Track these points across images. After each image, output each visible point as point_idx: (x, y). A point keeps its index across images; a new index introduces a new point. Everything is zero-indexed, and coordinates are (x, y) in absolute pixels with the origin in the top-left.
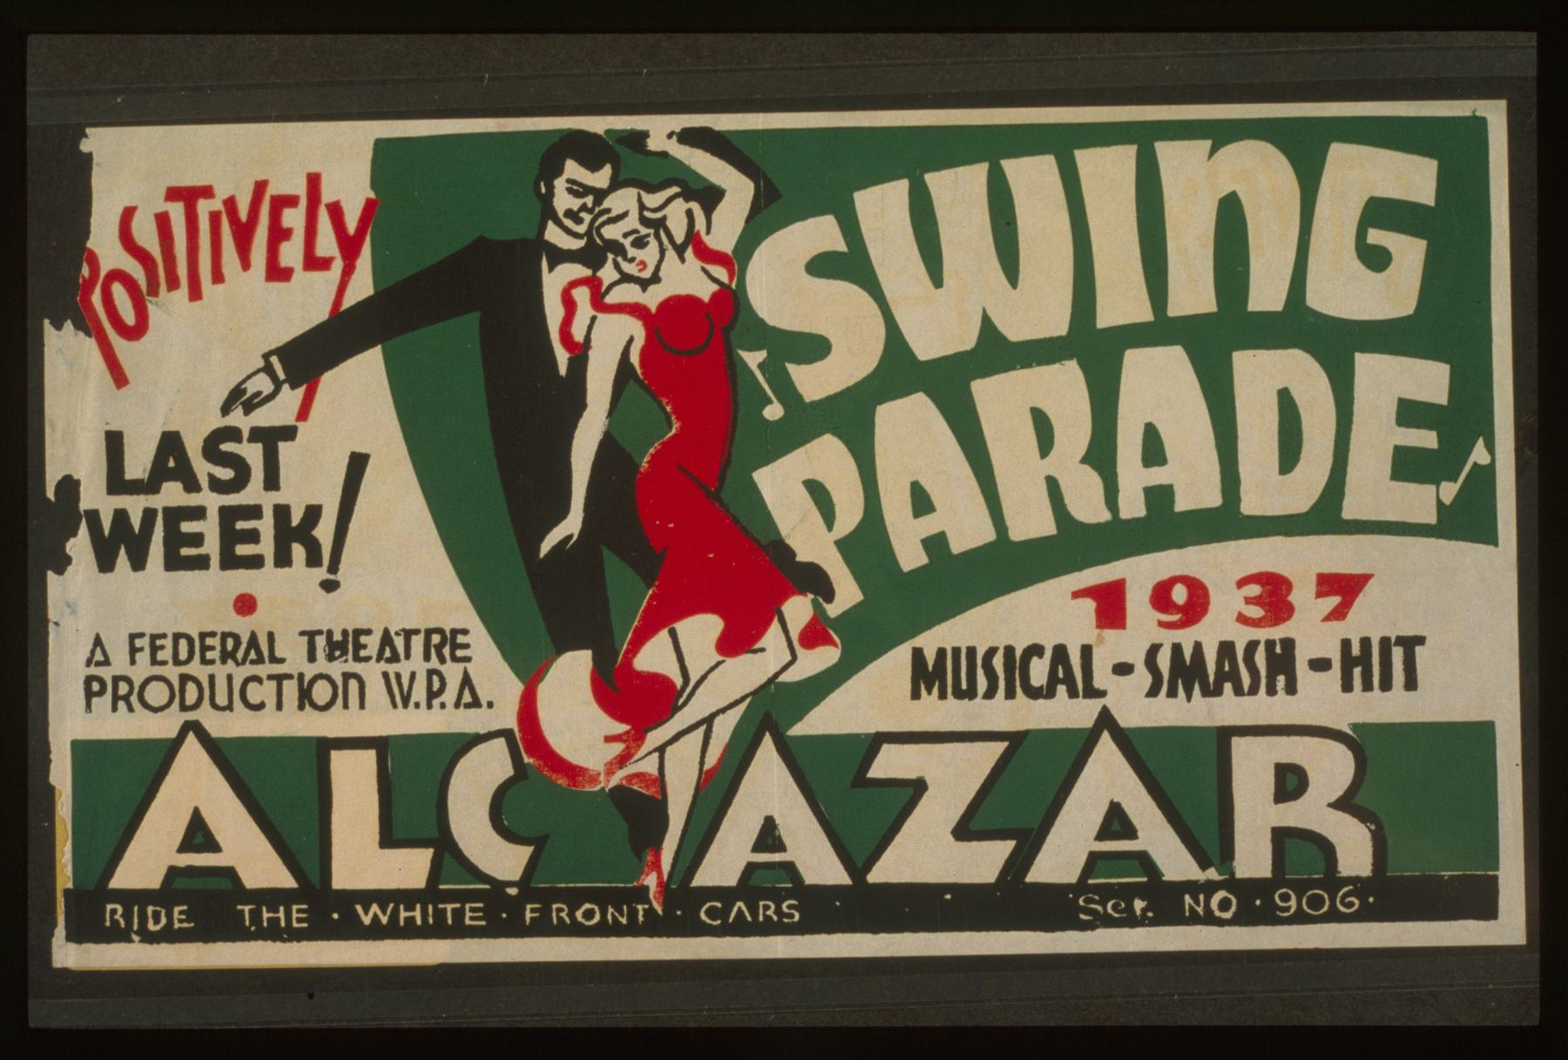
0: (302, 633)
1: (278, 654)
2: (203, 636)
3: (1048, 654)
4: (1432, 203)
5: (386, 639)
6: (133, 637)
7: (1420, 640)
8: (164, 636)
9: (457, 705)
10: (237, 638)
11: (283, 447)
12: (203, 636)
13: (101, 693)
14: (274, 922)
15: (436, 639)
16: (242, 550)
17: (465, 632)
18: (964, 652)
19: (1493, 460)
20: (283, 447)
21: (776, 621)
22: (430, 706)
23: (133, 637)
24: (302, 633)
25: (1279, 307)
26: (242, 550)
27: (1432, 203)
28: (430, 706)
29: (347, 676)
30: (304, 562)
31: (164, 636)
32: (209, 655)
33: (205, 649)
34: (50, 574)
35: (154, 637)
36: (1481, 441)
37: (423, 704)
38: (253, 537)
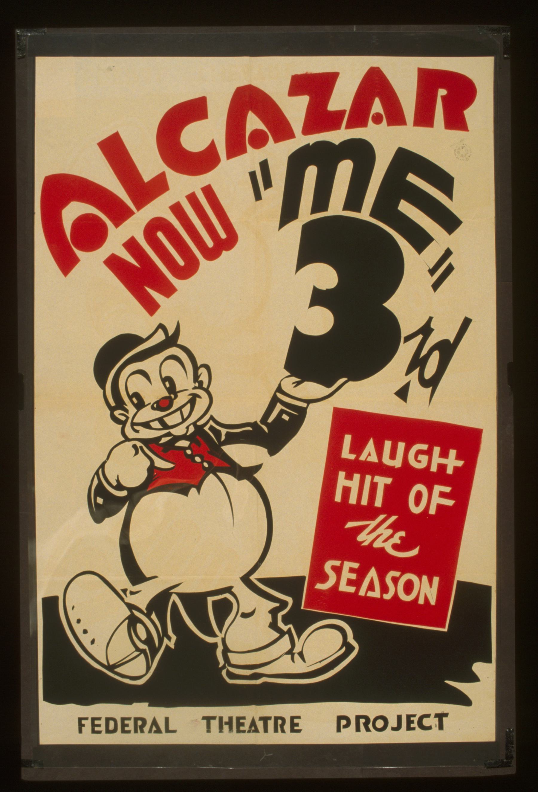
0: (204, 718)
2: (123, 719)
3: (153, 731)
5: (253, 723)
6: (80, 720)
7: (446, 715)
8: (129, 719)
10: (144, 721)
11: (444, 719)
12: (123, 719)
13: (347, 725)
14: (413, 722)
16: (97, 729)
17: (299, 717)
18: (139, 731)
19: (190, 425)
20: (444, 719)
23: (80, 720)
26: (97, 729)
30: (349, 578)
31: (129, 719)
33: (124, 725)
35: (93, 719)
36: (418, 369)
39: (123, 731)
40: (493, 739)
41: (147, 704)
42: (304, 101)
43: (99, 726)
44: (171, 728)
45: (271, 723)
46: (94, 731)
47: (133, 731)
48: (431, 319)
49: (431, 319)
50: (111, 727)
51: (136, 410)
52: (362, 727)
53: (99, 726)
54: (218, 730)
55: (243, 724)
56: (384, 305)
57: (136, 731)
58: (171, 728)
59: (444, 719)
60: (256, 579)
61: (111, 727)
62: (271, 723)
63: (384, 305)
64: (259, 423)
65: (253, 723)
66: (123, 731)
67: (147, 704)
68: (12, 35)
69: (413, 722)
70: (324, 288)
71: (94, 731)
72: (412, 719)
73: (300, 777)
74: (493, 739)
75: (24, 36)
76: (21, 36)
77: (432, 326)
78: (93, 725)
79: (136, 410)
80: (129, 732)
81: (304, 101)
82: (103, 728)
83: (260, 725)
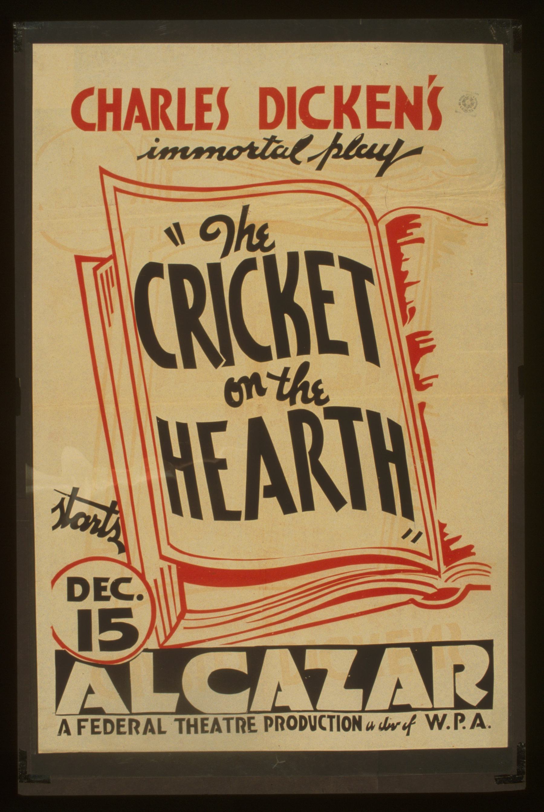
0: (164, 732)
1: (177, 723)
4: (325, 304)
5: (216, 722)
9: (472, 727)
11: (215, 436)
13: (271, 725)
15: (241, 723)
16: (96, 730)
20: (215, 436)
21: (248, 691)
22: (456, 728)
24: (164, 732)
25: (275, 498)
26: (96, 730)
27: (325, 304)
28: (456, 728)
29: (277, 718)
32: (122, 729)
34: (97, 534)
37: (452, 726)
38: (98, 727)
40: (506, 746)
43: (123, 726)
45: (233, 723)
46: (93, 732)
47: (128, 733)
51: (307, 651)
52: (134, 731)
53: (123, 726)
54: (235, 731)
55: (207, 725)
56: (354, 422)
57: (131, 733)
58: (163, 730)
60: (158, 419)
62: (233, 723)
63: (354, 422)
65: (216, 722)
68: (11, 32)
71: (93, 732)
74: (506, 746)
75: (21, 30)
76: (18, 30)
78: (93, 727)
79: (307, 651)
80: (99, 733)
82: (101, 729)
83: (223, 724)
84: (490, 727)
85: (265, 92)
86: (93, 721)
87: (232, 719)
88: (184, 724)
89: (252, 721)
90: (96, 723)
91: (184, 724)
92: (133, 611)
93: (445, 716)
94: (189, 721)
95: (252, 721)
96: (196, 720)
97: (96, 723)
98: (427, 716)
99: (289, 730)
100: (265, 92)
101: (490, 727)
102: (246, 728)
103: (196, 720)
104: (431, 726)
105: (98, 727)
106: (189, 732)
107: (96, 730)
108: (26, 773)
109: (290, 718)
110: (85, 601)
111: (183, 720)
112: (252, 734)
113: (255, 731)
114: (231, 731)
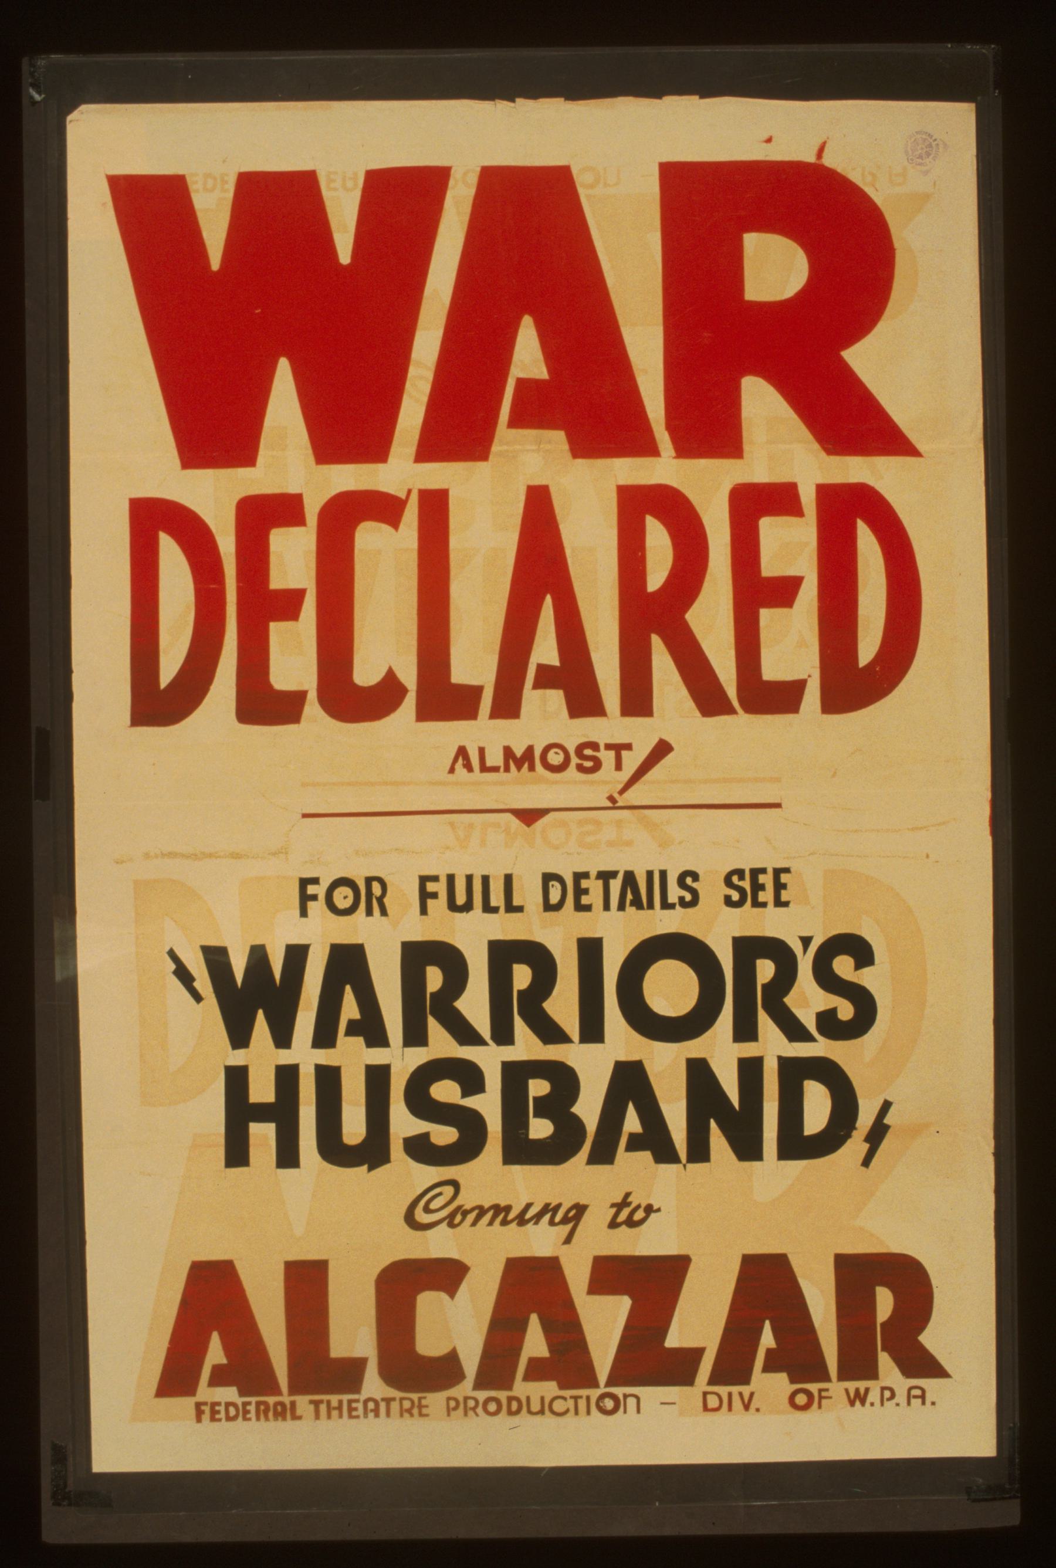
1: (312, 1407)
2: (579, 877)
13: (455, 1408)
33: (580, 892)
37: (877, 1402)
38: (356, 1409)
39: (580, 907)
41: (365, 1167)
42: (621, 1306)
44: (516, 902)
48: (866, 1162)
49: (866, 1162)
50: (555, 896)
52: (262, 1416)
58: (516, 902)
59: (625, 754)
61: (555, 896)
64: (410, 702)
66: (580, 907)
67: (365, 1167)
69: (218, 1412)
70: (84, 107)
72: (217, 1408)
73: (618, 670)
77: (866, 1146)
81: (621, 1306)
82: (222, 1415)
84: (933, 1403)
85: (548, 878)
86: (350, 1402)
87: (581, 1397)
88: (323, 1408)
89: (424, 1402)
90: (354, 1405)
91: (323, 1408)
92: (606, 1168)
93: (867, 1390)
94: (329, 1402)
95: (424, 1402)
96: (340, 1402)
97: (354, 1405)
98: (847, 1391)
99: (599, 1415)
100: (548, 878)
101: (933, 1403)
102: (415, 1411)
103: (340, 1402)
104: (852, 1403)
105: (356, 1409)
106: (329, 1417)
107: (354, 1413)
108: (65, 1486)
109: (276, 1404)
110: (482, 1156)
111: (321, 1402)
112: (422, 1419)
113: (427, 1415)
114: (392, 1414)
